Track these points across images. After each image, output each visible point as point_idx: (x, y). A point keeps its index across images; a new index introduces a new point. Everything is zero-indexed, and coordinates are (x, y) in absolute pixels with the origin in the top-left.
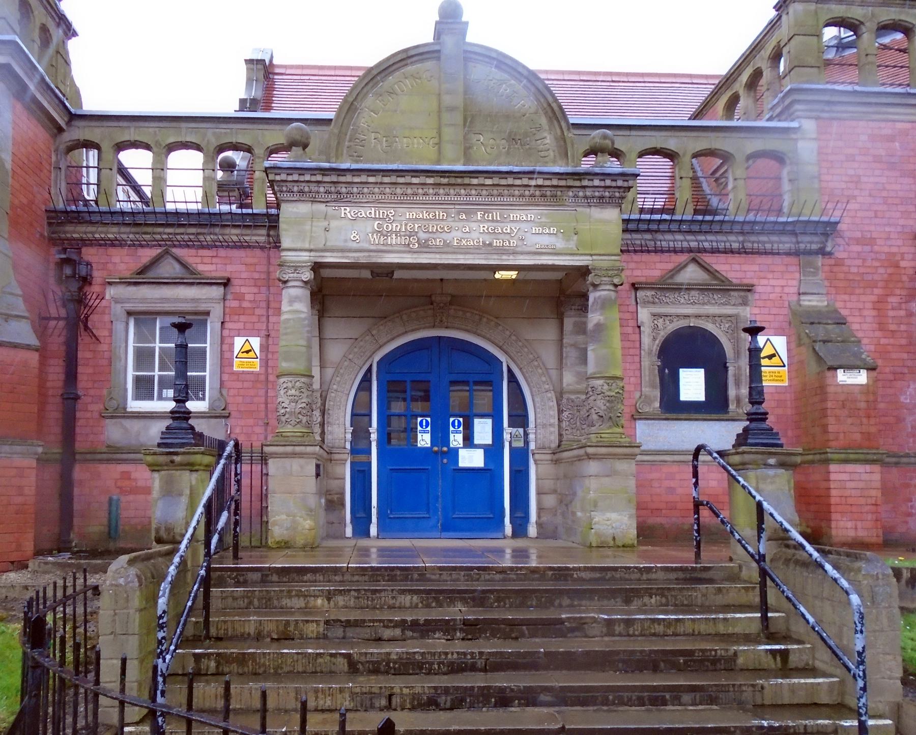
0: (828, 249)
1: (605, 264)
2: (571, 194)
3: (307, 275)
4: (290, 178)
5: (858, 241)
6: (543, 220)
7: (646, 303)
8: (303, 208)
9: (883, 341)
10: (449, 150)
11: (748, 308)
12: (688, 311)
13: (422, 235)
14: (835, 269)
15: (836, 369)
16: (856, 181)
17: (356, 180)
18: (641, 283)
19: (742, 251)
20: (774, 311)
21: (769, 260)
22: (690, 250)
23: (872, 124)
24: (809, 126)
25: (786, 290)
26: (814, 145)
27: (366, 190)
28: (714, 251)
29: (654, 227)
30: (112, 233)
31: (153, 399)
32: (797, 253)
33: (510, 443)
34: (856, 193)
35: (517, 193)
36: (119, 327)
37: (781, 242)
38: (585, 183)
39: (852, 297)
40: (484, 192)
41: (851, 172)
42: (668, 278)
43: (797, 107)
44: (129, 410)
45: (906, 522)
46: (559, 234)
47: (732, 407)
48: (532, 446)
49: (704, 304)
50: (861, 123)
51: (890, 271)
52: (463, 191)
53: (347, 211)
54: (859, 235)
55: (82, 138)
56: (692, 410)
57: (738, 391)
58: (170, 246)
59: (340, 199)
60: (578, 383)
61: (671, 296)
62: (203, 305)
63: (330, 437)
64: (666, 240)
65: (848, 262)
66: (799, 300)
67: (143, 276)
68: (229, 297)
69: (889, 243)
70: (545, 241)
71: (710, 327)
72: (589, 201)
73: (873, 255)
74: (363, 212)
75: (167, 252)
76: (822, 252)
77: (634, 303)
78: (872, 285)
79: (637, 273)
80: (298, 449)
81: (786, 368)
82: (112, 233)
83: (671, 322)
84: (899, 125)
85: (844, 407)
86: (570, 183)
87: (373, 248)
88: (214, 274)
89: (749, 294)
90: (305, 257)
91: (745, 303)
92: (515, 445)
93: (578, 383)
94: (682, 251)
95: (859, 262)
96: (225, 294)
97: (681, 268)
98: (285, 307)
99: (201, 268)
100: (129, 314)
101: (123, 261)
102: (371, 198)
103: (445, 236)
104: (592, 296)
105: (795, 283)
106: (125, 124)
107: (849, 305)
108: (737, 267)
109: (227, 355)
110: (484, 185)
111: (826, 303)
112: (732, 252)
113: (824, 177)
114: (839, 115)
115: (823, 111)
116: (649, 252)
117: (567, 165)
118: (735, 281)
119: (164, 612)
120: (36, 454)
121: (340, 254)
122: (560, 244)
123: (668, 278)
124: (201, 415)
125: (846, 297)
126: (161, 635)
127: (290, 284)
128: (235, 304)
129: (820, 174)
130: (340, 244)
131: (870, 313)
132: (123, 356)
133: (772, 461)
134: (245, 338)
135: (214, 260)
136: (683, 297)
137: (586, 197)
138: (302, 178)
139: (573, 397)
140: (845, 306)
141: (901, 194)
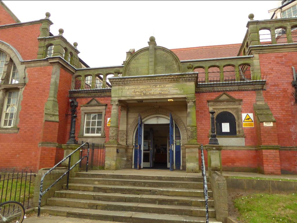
0: (264, 88)
2: (181, 79)
3: (117, 103)
4: (114, 81)
5: (273, 86)
6: (174, 86)
7: (211, 106)
8: (117, 87)
9: (283, 113)
10: (151, 71)
11: (241, 106)
13: (144, 92)
14: (267, 94)
15: (263, 122)
16: (272, 69)
17: (128, 80)
18: (209, 100)
19: (239, 90)
20: (249, 106)
21: (246, 92)
22: (224, 91)
24: (256, 56)
26: (258, 61)
27: (131, 82)
28: (230, 91)
29: (213, 85)
30: (83, 95)
31: (89, 133)
32: (255, 90)
33: (176, 144)
34: (272, 72)
35: (167, 80)
36: (83, 116)
38: (184, 76)
39: (273, 101)
40: (156, 81)
41: (270, 67)
42: (217, 99)
43: (252, 51)
44: (84, 136)
45: (295, 168)
46: (179, 90)
47: (237, 133)
48: (181, 145)
49: (228, 105)
51: (284, 93)
52: (154, 81)
53: (127, 87)
54: (273, 84)
55: (78, 75)
56: (226, 134)
58: (94, 97)
59: (125, 85)
62: (101, 111)
63: (129, 142)
64: (216, 89)
65: (270, 92)
66: (256, 103)
67: (88, 104)
68: (107, 108)
69: (283, 85)
70: (175, 91)
71: (230, 111)
72: (186, 81)
74: (130, 87)
75: (93, 99)
76: (262, 89)
77: (208, 106)
78: (279, 97)
79: (209, 98)
80: (112, 145)
81: (253, 122)
82: (83, 95)
83: (219, 110)
84: (284, 53)
85: (266, 133)
86: (180, 77)
87: (132, 96)
88: (104, 103)
89: (241, 102)
90: (117, 99)
91: (240, 104)
92: (177, 144)
95: (274, 92)
96: (106, 108)
97: (91, 101)
98: (112, 111)
99: (101, 102)
100: (85, 113)
101: (84, 101)
102: (132, 84)
103: (150, 92)
104: (188, 104)
105: (255, 98)
106: (87, 71)
107: (272, 103)
108: (237, 95)
109: (106, 123)
110: (159, 79)
111: (264, 103)
112: (235, 91)
116: (212, 92)
117: (180, 72)
118: (237, 99)
119: (42, 181)
120: (56, 146)
121: (124, 98)
122: (179, 92)
123: (217, 99)
124: (210, 137)
125: (271, 101)
126: (41, 186)
127: (113, 105)
128: (108, 110)
130: (125, 95)
131: (278, 106)
132: (83, 123)
133: (214, 148)
134: (247, 114)
135: (104, 100)
138: (116, 80)
141: (286, 72)
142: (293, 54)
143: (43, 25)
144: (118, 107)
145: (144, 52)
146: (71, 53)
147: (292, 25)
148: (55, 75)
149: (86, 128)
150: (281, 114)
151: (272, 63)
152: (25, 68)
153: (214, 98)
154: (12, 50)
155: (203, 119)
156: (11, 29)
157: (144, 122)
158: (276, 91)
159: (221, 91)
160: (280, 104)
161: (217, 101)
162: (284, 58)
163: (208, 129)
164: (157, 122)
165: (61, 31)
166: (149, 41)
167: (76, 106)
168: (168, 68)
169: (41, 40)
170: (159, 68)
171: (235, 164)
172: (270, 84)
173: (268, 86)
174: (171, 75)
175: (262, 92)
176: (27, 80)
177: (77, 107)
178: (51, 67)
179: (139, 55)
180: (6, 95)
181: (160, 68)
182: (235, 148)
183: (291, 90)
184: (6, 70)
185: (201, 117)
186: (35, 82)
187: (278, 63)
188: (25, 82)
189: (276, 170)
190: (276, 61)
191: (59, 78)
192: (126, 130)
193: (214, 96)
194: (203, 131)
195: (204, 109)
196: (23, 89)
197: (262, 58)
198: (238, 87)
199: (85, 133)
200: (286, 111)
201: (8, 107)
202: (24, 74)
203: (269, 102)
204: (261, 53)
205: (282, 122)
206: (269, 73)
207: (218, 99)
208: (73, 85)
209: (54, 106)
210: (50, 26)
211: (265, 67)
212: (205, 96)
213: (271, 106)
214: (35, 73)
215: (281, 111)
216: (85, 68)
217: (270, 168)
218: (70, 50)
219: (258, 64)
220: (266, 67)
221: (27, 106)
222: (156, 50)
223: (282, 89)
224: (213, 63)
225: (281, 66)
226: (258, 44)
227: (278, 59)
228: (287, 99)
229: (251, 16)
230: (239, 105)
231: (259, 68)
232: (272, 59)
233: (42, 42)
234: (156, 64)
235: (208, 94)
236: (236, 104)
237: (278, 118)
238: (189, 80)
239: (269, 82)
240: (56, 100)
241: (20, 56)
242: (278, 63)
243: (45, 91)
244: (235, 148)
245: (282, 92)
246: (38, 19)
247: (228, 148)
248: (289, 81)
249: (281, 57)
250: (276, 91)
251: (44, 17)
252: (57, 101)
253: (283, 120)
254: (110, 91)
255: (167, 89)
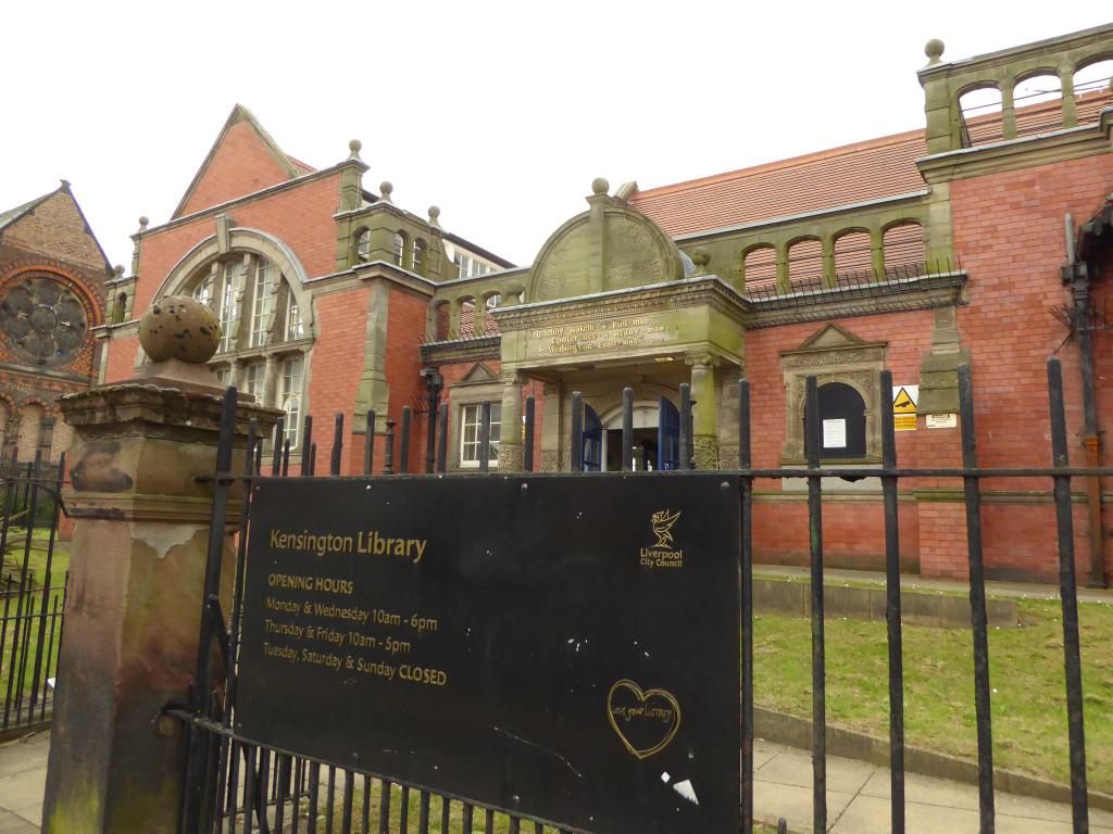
1: (696, 349)
2: (671, 300)
5: (995, 288)
7: (790, 367)
8: (513, 335)
9: (1023, 381)
12: (826, 370)
14: (971, 317)
15: (925, 415)
16: (993, 231)
19: (878, 312)
20: (909, 362)
21: (902, 316)
22: (829, 318)
23: (1008, 174)
24: (942, 189)
25: (921, 342)
26: (947, 206)
28: (848, 316)
30: (453, 355)
32: (931, 307)
34: (992, 241)
36: (454, 415)
37: (910, 300)
38: (679, 291)
41: (987, 223)
47: (869, 452)
50: (997, 176)
53: (537, 333)
54: (996, 281)
57: (873, 437)
60: (731, 437)
61: (812, 359)
64: (807, 313)
65: (984, 309)
67: (466, 381)
70: (658, 336)
73: (1012, 299)
76: (956, 302)
79: (786, 342)
84: (1038, 169)
85: (933, 450)
93: (731, 437)
94: (821, 319)
95: (997, 307)
97: (820, 335)
100: (462, 405)
101: (458, 372)
104: (694, 372)
107: (986, 349)
108: (872, 327)
111: (958, 351)
113: (957, 234)
114: (969, 174)
115: (952, 174)
116: (792, 323)
122: (667, 338)
125: (983, 342)
127: (695, 367)
129: (953, 231)
130: (534, 355)
131: (1008, 355)
134: (900, 388)
136: (823, 359)
137: (682, 301)
139: (728, 448)
140: (981, 352)
141: (1042, 235)
142: (1075, 169)
143: (346, 178)
144: (518, 389)
145: (579, 229)
146: (420, 242)
147: (1078, 59)
148: (374, 311)
149: (465, 446)
150: (1015, 382)
151: (993, 209)
152: (313, 298)
153: (802, 341)
154: (282, 253)
155: (767, 409)
156: (278, 197)
157: (608, 424)
158: (1001, 305)
159: (821, 319)
160: (1014, 350)
161: (808, 351)
162: (1037, 188)
163: (780, 439)
164: (645, 423)
165: (386, 189)
166: (593, 194)
167: (439, 388)
168: (640, 269)
169: (341, 219)
170: (616, 269)
171: (857, 547)
172: (982, 283)
173: (977, 290)
174: (643, 291)
175: (954, 314)
176: (318, 330)
177: (442, 388)
178: (366, 290)
179: (567, 237)
180: (279, 369)
181: (618, 271)
182: (857, 497)
183: (1058, 298)
184: (274, 308)
185: (761, 403)
186: (335, 332)
187: (1016, 206)
188: (313, 334)
189: (956, 564)
190: (1009, 200)
191: (386, 317)
192: (556, 448)
193: (799, 336)
194: (765, 445)
195: (770, 379)
196: (311, 352)
197: (962, 195)
198: (873, 302)
199: (465, 459)
200: (1035, 371)
201: (285, 398)
202: (310, 315)
203: (975, 343)
204: (959, 176)
205: (1016, 409)
206: (981, 243)
207: (812, 346)
208: (431, 329)
209: (376, 392)
210: (361, 176)
211: (969, 226)
212: (774, 338)
213: (984, 356)
214: (333, 309)
215: (1017, 374)
216: (501, 270)
217: (939, 559)
218: (414, 233)
219: (947, 217)
220: (973, 225)
221: (321, 396)
222: (609, 217)
223: (1023, 299)
224: (799, 230)
225: (1026, 217)
226: (948, 147)
227: (1016, 192)
228: (1040, 331)
229: (935, 50)
230: (874, 360)
231: (949, 232)
232: (995, 196)
233: (345, 225)
234: (607, 262)
235: (784, 329)
236: (866, 358)
237: (1005, 396)
238: (693, 299)
239: (979, 276)
240: (382, 376)
241: (300, 266)
242: (1016, 206)
243: (357, 355)
244: (857, 497)
245: (1025, 308)
246: (332, 164)
247: (836, 497)
248: (1052, 268)
249: (1030, 184)
250: (1001, 305)
251: (344, 155)
252: (385, 379)
253: (1020, 402)
254: (496, 342)
255: (636, 330)
